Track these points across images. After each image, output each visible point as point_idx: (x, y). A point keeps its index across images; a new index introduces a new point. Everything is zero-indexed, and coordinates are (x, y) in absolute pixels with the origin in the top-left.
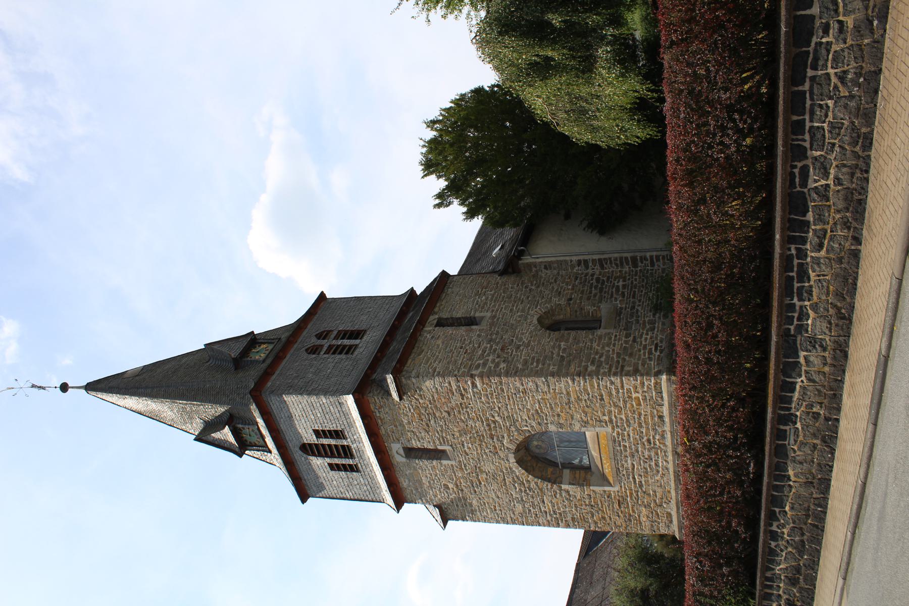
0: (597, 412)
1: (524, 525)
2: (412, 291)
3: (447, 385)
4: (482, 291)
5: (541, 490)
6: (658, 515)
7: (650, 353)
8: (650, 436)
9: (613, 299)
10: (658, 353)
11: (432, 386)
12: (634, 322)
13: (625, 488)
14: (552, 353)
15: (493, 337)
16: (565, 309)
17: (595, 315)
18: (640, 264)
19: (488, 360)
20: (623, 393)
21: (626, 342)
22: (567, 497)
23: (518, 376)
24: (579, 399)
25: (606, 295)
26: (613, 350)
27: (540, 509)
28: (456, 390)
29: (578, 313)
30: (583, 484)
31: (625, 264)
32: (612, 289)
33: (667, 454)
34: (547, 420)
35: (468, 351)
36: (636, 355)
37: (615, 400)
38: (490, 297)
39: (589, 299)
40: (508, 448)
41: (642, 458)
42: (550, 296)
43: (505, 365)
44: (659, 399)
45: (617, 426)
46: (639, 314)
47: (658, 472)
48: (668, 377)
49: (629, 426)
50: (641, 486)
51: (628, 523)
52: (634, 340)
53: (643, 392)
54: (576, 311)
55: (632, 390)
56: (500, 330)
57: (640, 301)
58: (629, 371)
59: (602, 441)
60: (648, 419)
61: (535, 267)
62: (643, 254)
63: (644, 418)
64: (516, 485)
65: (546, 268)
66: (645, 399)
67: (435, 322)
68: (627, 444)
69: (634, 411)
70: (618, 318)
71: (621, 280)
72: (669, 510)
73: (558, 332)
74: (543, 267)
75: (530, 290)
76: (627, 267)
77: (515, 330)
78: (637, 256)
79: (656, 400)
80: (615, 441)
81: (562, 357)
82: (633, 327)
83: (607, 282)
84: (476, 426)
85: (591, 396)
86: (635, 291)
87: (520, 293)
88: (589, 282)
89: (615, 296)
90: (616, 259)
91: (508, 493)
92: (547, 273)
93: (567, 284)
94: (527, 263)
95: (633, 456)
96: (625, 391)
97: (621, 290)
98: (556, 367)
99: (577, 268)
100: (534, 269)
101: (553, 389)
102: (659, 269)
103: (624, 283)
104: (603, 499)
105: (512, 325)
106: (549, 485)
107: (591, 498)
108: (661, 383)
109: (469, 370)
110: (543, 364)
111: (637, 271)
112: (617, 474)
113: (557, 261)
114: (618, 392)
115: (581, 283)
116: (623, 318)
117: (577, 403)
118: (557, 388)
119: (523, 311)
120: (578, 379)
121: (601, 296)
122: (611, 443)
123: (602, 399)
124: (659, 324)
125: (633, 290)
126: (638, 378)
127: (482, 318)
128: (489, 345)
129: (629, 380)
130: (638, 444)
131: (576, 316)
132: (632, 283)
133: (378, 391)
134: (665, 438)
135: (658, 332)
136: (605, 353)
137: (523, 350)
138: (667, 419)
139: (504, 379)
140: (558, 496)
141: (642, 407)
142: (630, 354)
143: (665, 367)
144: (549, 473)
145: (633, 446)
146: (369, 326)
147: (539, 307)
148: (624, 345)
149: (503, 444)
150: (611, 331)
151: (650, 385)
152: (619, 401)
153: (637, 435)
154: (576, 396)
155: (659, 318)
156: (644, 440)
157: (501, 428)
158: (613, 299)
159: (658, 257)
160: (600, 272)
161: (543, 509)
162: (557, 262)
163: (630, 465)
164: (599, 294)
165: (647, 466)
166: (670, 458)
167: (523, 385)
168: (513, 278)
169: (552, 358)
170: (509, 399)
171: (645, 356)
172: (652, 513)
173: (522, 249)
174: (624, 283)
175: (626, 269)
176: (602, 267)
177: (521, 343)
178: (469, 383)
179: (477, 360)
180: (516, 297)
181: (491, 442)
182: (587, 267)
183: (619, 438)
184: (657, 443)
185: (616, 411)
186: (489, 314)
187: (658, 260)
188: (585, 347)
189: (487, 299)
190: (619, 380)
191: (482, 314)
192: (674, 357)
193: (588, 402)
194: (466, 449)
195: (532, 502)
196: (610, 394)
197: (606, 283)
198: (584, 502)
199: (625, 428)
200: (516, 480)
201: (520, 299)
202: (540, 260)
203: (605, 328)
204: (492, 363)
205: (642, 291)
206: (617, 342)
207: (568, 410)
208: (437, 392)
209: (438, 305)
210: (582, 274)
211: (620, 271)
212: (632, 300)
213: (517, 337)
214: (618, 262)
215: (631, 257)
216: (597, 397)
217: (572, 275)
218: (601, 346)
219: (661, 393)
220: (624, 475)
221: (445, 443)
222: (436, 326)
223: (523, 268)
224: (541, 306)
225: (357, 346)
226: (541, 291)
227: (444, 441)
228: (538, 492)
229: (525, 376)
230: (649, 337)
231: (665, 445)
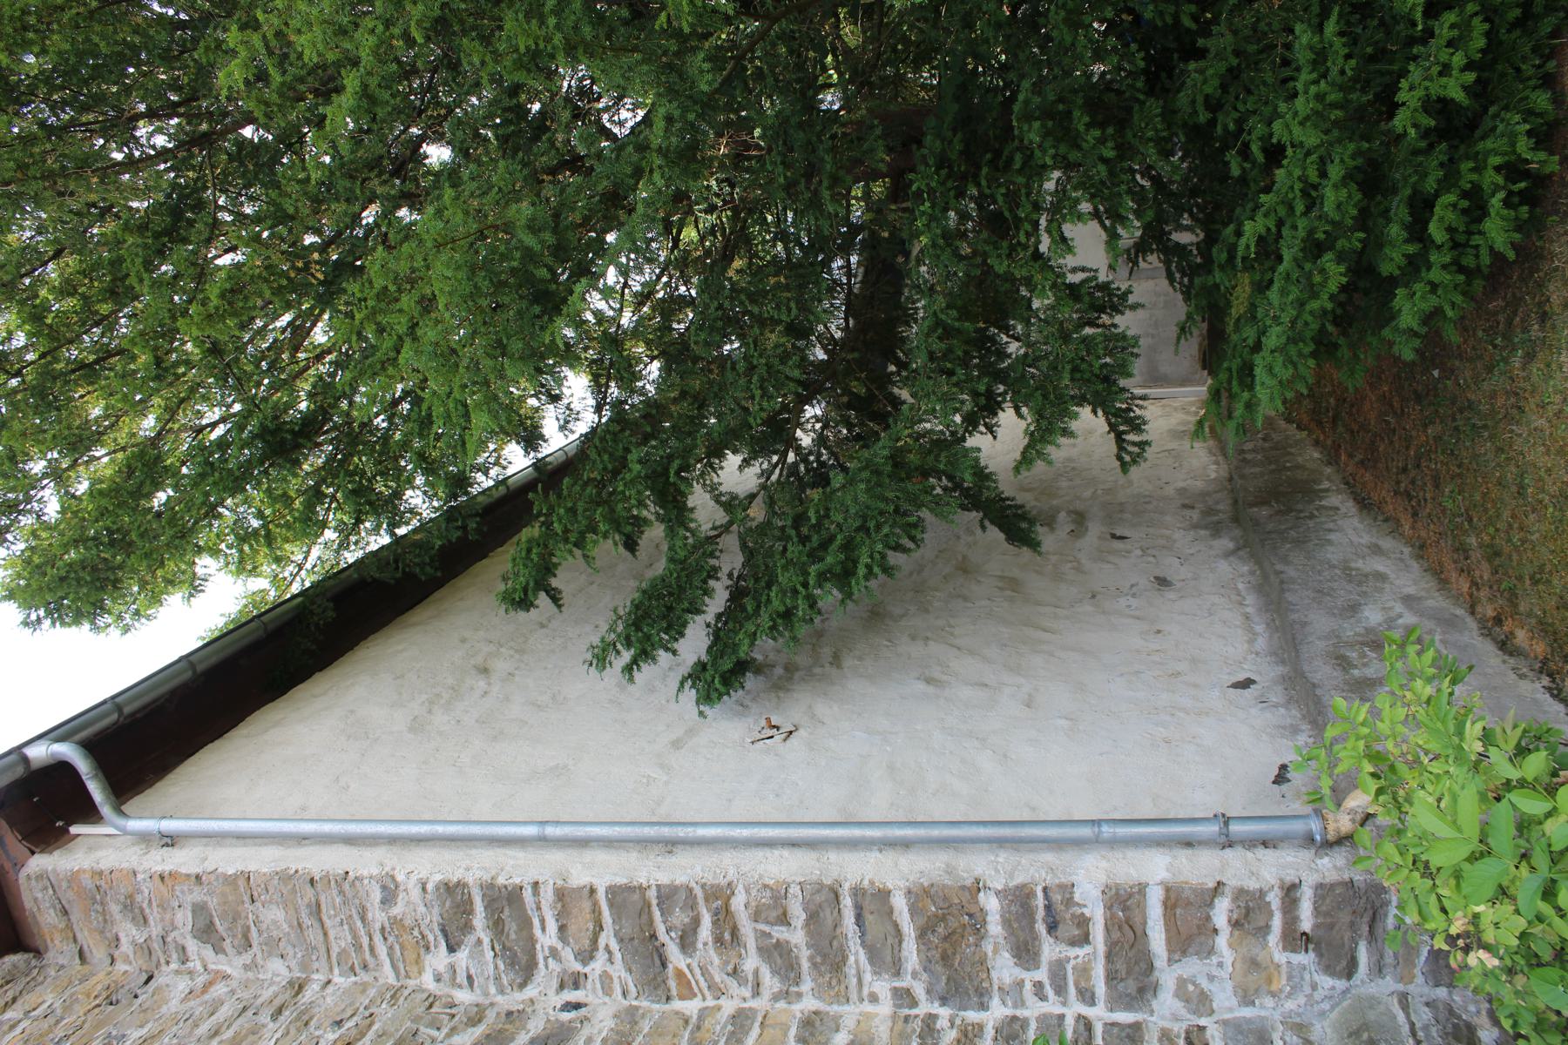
18: (1004, 968)
31: (857, 955)
62: (1034, 870)
65: (206, 932)
74: (184, 919)
76: (882, 987)
90: (774, 908)
94: (74, 877)
99: (439, 959)
100: (129, 933)
182: (523, 966)
202: (182, 860)
214: (797, 936)
215: (919, 896)
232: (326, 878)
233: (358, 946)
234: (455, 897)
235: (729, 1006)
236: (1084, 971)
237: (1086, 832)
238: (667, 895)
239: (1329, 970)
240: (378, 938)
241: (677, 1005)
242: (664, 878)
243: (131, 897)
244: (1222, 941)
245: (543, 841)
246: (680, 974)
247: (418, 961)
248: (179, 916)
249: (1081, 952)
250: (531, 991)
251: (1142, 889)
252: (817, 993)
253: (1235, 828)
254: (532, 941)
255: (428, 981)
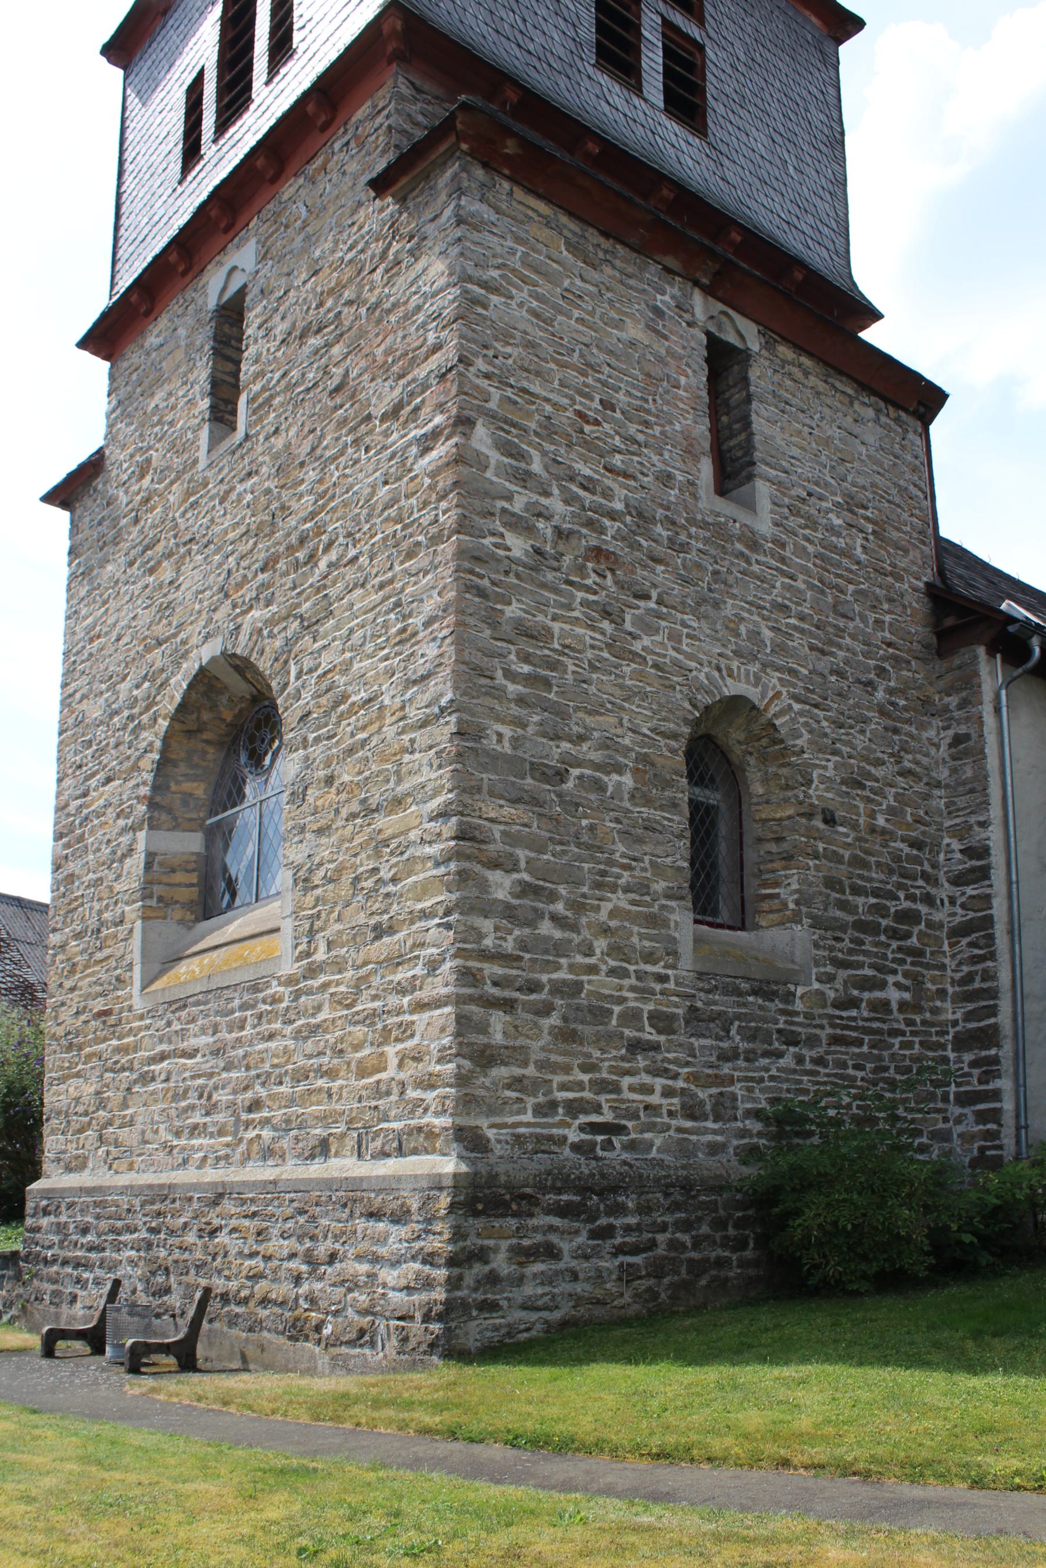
0: (339, 919)
1: (60, 734)
2: (872, 315)
3: (431, 337)
4: (867, 519)
5: (136, 767)
6: (81, 1131)
7: (574, 1108)
8: (271, 1109)
9: (829, 969)
10: (573, 1136)
11: (427, 289)
12: (725, 1045)
13: (140, 1029)
14: (581, 738)
15: (659, 529)
16: (786, 800)
17: (765, 906)
18: (968, 1057)
19: (547, 494)
20: (399, 1012)
21: (631, 1017)
22: (119, 853)
23: (459, 598)
24: (379, 844)
25: (847, 944)
26: (593, 969)
27: (93, 775)
28: (414, 380)
29: (773, 847)
30: (151, 897)
31: (970, 1006)
32: (872, 966)
33: (222, 1163)
34: (317, 740)
35: (587, 428)
36: (565, 1053)
37: (376, 981)
38: (841, 543)
39: (831, 883)
40: (238, 628)
41: (211, 1083)
42: (845, 749)
43: (517, 553)
44: (378, 1143)
45: (297, 995)
46: (764, 1062)
47: (178, 1134)
48: (448, 1182)
49: (297, 1035)
50: (147, 1078)
51: (64, 1042)
52: (636, 1047)
53: (403, 1084)
54: (779, 840)
55: (410, 1044)
56: (692, 556)
57: (820, 1061)
58: (483, 1029)
59: (258, 946)
60: (319, 1103)
61: (963, 705)
62: (1007, 1065)
63: (320, 1090)
64: (147, 684)
65: (958, 740)
66: (379, 1091)
67: (731, 338)
68: (247, 1032)
69: (341, 1051)
70: (745, 986)
71: (907, 996)
72: (91, 1165)
73: (684, 769)
74: (963, 729)
75: (869, 685)
76: (959, 1015)
77: (694, 612)
78: (999, 1046)
79: (377, 1134)
80: (255, 988)
81: (561, 776)
82: (707, 1042)
83: (900, 949)
84: (301, 496)
85: (391, 888)
86: (859, 1043)
87: (859, 647)
88: (900, 886)
89: (843, 974)
90: (988, 976)
91: (127, 666)
92: (937, 746)
93: (891, 811)
94: (976, 674)
95: (216, 1053)
96: (408, 1017)
97: (866, 995)
98: (507, 748)
99: (956, 845)
100: (953, 701)
101: (412, 741)
102: (946, 1120)
103: (894, 1006)
104: (114, 964)
105: (717, 605)
106: (145, 791)
107: (116, 925)
108: (434, 1151)
109: (492, 416)
110: (521, 701)
111: (943, 1047)
112: (170, 1003)
113: (986, 777)
114: (401, 990)
115: (897, 859)
116: (745, 1005)
117: (367, 842)
118: (417, 755)
119: (780, 649)
120: (447, 833)
121: (843, 928)
122: (247, 975)
123: (380, 932)
124: (715, 1132)
125: (867, 1039)
126: (451, 1066)
127: (750, 505)
128: (619, 506)
129: (443, 1030)
130: (248, 1068)
131: (760, 840)
132: (894, 1033)
133: (420, 118)
134: (264, 1158)
135: (679, 1130)
136: (576, 939)
137: (593, 628)
138: (316, 1170)
139: (447, 549)
140: (121, 822)
141: (353, 1082)
142: (574, 1032)
143: (501, 1169)
144: (187, 786)
145: (241, 1052)
146: (723, 148)
147: (796, 707)
148: (617, 1009)
149: (251, 608)
150: (687, 962)
151: (426, 1110)
152: (375, 997)
153: (274, 1066)
154: (389, 832)
155: (744, 1133)
156: (258, 1088)
157: (294, 588)
158: (829, 969)
159: (995, 1115)
160: (941, 925)
161: (93, 783)
162: (983, 778)
163: (193, 1042)
164: (851, 919)
165: (192, 1099)
166: (211, 1175)
167: (427, 624)
168: (919, 630)
169: (556, 737)
170: (382, 586)
171: (563, 1087)
172: (86, 1113)
173: (1030, 652)
174: (894, 1006)
175: (951, 1012)
176: (959, 932)
177: (628, 626)
178: (439, 419)
179: (544, 453)
180: (840, 631)
181: (254, 568)
182: (958, 880)
183: (264, 1002)
184: (251, 1134)
185: (342, 988)
186: (764, 525)
187: (982, 1117)
188: (611, 863)
189: (831, 529)
190: (444, 991)
191: (764, 504)
192: (551, 1197)
193: (369, 884)
194: (240, 488)
195: (108, 744)
196: (396, 961)
197: (895, 944)
198: (107, 906)
199: (291, 1022)
200: (157, 679)
201: (831, 643)
202: (989, 719)
203: (698, 940)
204: (528, 507)
205: (856, 1067)
206: (633, 981)
207: (344, 812)
208: (406, 317)
209: (805, 360)
210: (935, 866)
211: (942, 993)
212: (824, 1034)
213: (660, 616)
214: (977, 985)
215: (995, 1027)
216: (386, 912)
217: (932, 830)
218: (613, 924)
219: (400, 1152)
220: (169, 1024)
221: (254, 413)
222: (708, 334)
223: (957, 661)
224: (801, 713)
225: (637, 88)
226: (866, 721)
227: (260, 407)
228: (129, 758)
229: (459, 624)
230: (655, 1099)
231: (247, 1157)
232: (987, 795)
233: (958, 810)
234: (983, 852)
235: (947, 961)
236: (968, 1083)
237: (1021, 1082)
238: (991, 938)
239: (971, 1160)
240: (962, 819)
241: (946, 942)
242: (997, 935)
243: (970, 703)
244: (981, 1127)
245: (1010, 883)
246: (958, 942)
247: (954, 836)
248: (964, 727)
249: (976, 1082)
250: (946, 885)
251: (1001, 1101)
252: (954, 993)
253: (1023, 1131)
254: (968, 885)
255: (947, 840)
